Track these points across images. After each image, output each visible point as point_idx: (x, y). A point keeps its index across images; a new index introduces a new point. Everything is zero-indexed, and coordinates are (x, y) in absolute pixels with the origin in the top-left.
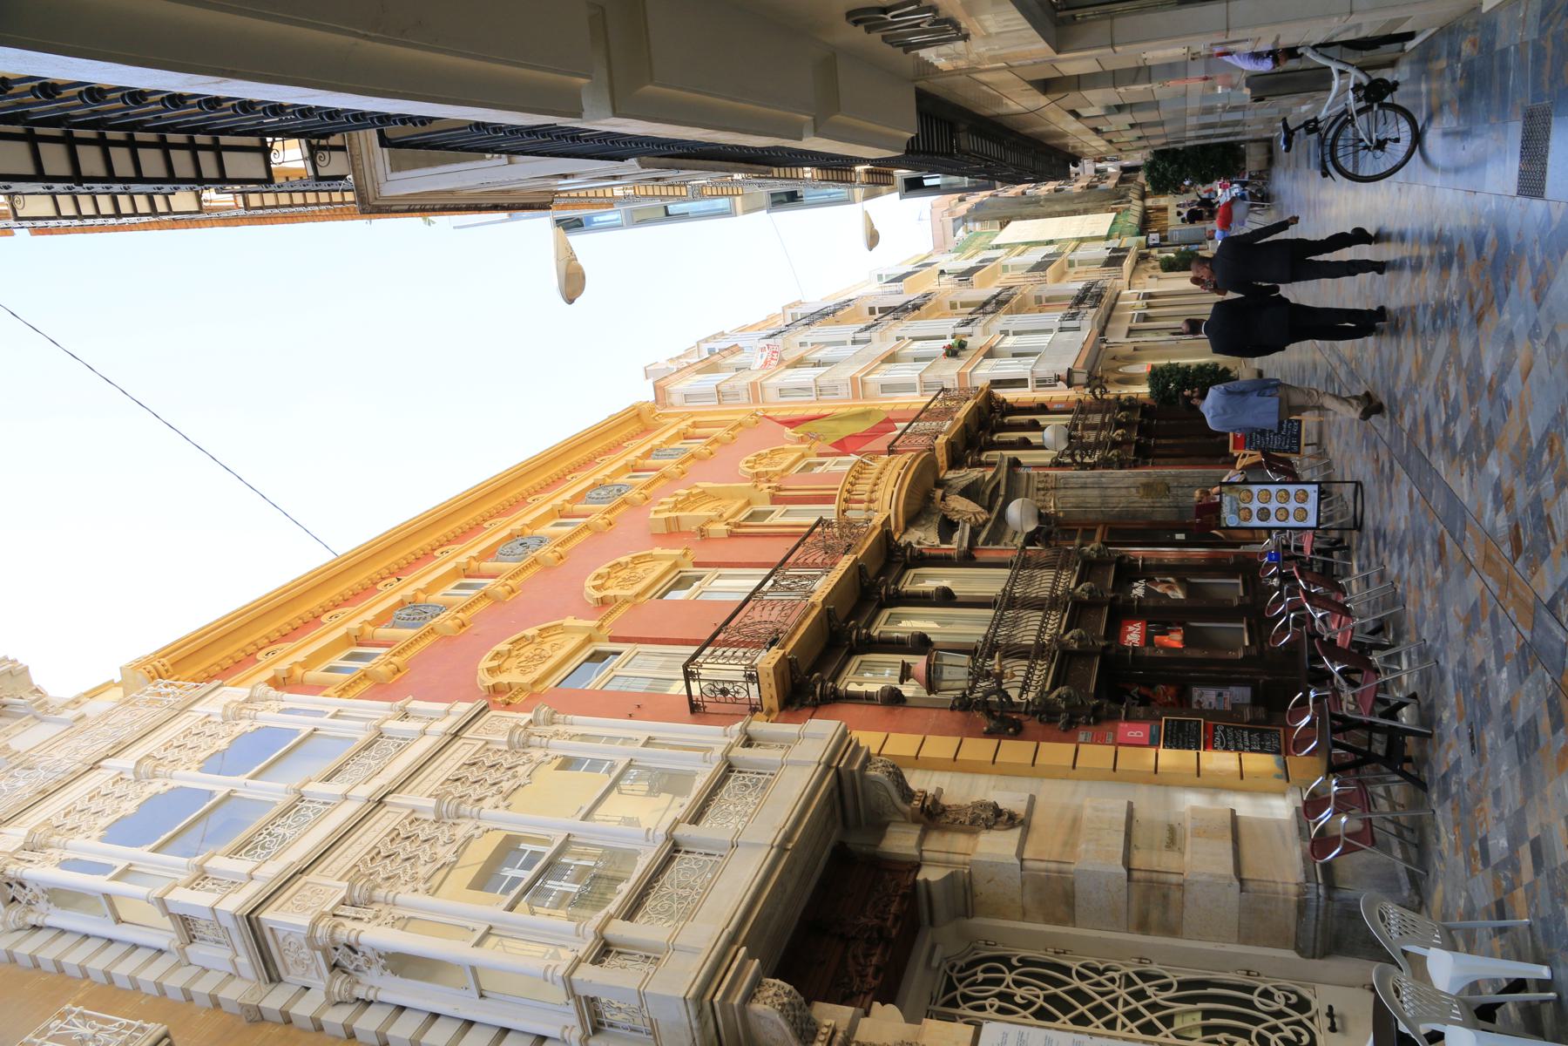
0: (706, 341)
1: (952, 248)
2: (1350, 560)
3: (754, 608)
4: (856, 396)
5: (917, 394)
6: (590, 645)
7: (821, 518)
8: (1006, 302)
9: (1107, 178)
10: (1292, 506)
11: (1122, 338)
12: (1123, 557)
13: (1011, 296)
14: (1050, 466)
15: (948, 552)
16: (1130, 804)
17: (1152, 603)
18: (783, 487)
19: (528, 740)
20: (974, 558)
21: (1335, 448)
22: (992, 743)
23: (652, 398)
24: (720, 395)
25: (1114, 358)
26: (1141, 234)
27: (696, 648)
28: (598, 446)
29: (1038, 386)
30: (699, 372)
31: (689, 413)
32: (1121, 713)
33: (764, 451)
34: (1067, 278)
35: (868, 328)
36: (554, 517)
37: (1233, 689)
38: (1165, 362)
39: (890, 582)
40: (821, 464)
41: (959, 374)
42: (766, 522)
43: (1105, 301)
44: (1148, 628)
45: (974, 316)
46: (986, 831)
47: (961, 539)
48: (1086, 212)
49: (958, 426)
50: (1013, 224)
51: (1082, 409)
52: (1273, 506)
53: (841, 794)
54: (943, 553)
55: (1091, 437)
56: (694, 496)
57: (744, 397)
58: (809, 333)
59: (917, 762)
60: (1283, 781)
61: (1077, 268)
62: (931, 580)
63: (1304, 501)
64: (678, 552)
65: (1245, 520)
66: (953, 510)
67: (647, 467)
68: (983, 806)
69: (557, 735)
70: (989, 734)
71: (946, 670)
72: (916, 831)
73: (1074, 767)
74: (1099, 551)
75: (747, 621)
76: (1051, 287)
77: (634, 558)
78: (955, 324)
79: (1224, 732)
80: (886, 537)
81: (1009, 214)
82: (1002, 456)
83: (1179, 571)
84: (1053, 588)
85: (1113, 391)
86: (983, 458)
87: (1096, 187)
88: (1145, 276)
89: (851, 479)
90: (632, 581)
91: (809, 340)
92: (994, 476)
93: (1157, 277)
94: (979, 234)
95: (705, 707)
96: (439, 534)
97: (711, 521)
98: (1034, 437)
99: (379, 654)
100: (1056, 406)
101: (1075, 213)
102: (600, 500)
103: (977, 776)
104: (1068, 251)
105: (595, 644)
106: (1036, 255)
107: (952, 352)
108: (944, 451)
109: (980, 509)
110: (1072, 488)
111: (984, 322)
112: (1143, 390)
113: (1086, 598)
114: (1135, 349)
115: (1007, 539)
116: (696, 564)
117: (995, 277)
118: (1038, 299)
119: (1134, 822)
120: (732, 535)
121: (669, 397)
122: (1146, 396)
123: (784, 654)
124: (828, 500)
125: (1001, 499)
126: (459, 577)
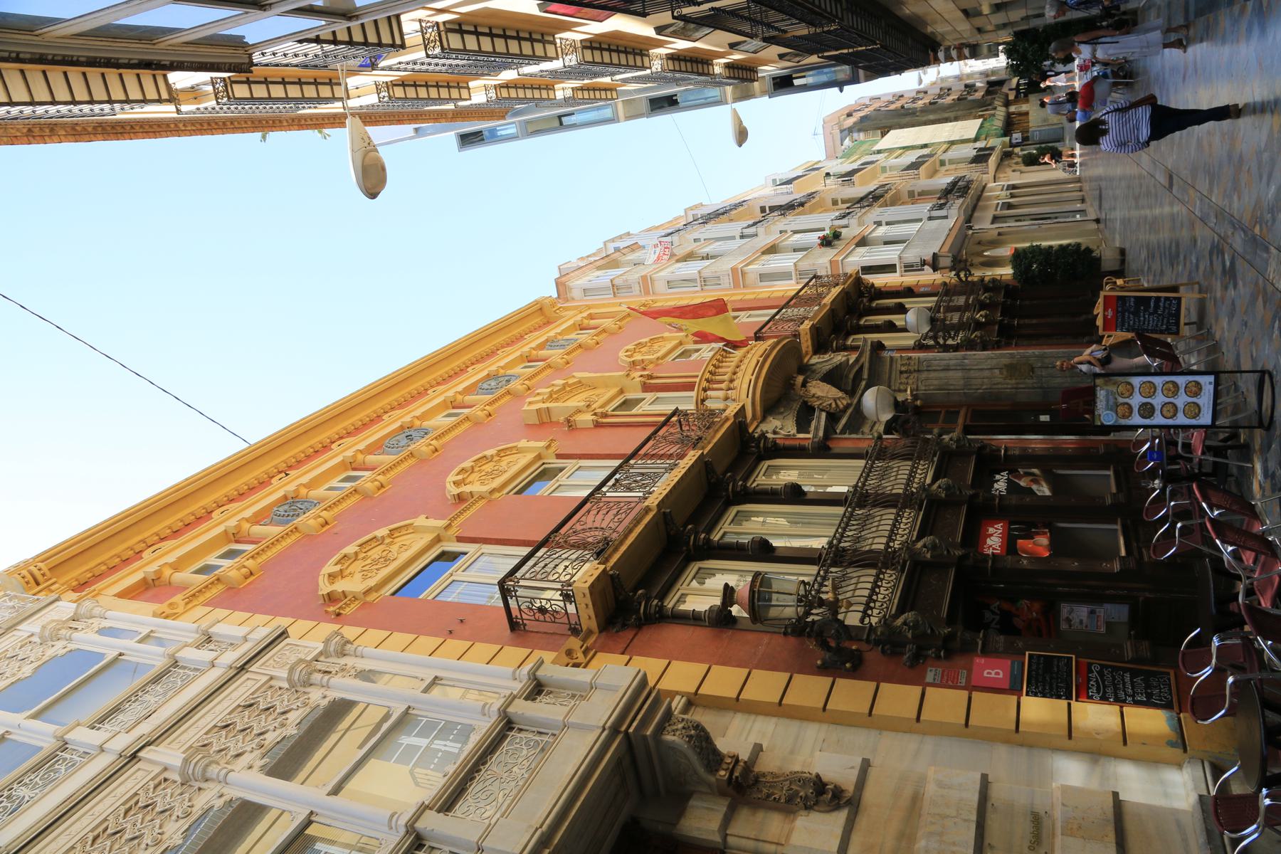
0: (613, 240)
1: (839, 155)
2: (1250, 460)
3: (589, 512)
4: (736, 286)
5: (793, 282)
6: (439, 545)
7: (677, 409)
8: (882, 196)
9: (976, 91)
10: (1181, 400)
11: (986, 225)
12: (983, 447)
13: (886, 192)
14: (914, 349)
15: (802, 443)
16: (984, 778)
17: (1014, 500)
18: (655, 375)
19: (309, 679)
20: (829, 448)
21: (1223, 328)
22: (824, 682)
23: (555, 295)
24: (615, 288)
25: (979, 243)
26: (1005, 135)
27: (528, 549)
28: (501, 339)
29: (906, 271)
30: (599, 268)
31: (587, 306)
32: (977, 643)
33: (644, 340)
34: (939, 175)
35: (755, 224)
36: (447, 408)
37: (1108, 606)
38: (1027, 245)
39: (738, 478)
40: (697, 350)
41: (831, 262)
42: (634, 411)
43: (971, 192)
44: (1010, 529)
45: (851, 210)
46: (803, 813)
47: (817, 429)
48: (956, 119)
49: (825, 311)
50: (892, 132)
51: (947, 291)
52: (1158, 400)
53: (634, 761)
54: (797, 443)
55: (955, 318)
56: (570, 385)
57: (636, 288)
58: (703, 230)
59: (737, 705)
60: (1179, 751)
61: (947, 167)
62: (787, 473)
63: (1196, 394)
64: (542, 444)
65: (1124, 417)
66: (813, 396)
67: (539, 358)
68: (800, 779)
69: (343, 670)
70: (824, 670)
71: (775, 596)
72: (721, 807)
73: (918, 719)
74: (958, 440)
75: (578, 527)
76: (923, 182)
77: (499, 451)
78: (833, 217)
79: (1101, 673)
80: (740, 425)
81: (889, 125)
82: (865, 340)
83: (1047, 463)
84: (907, 485)
85: (977, 274)
86: (849, 342)
87: (966, 99)
88: (1009, 170)
89: (711, 368)
90: (492, 475)
91: (702, 237)
92: (857, 360)
93: (1020, 171)
94: (863, 142)
95: (525, 625)
96: (339, 427)
97: (579, 411)
98: (898, 320)
99: (244, 551)
100: (922, 290)
101: (946, 120)
102: (489, 391)
103: (805, 724)
104: (940, 152)
105: (443, 544)
106: (911, 157)
107: (826, 242)
108: (588, 600)
109: (840, 394)
110: (935, 370)
111: (859, 214)
112: (1006, 272)
113: (943, 495)
114: (1000, 234)
115: (866, 429)
116: (559, 456)
117: (874, 177)
118: (911, 194)
119: (989, 805)
120: (598, 425)
121: (570, 292)
122: (1009, 277)
123: (604, 570)
124: (689, 387)
125: (864, 383)
126: (346, 470)
